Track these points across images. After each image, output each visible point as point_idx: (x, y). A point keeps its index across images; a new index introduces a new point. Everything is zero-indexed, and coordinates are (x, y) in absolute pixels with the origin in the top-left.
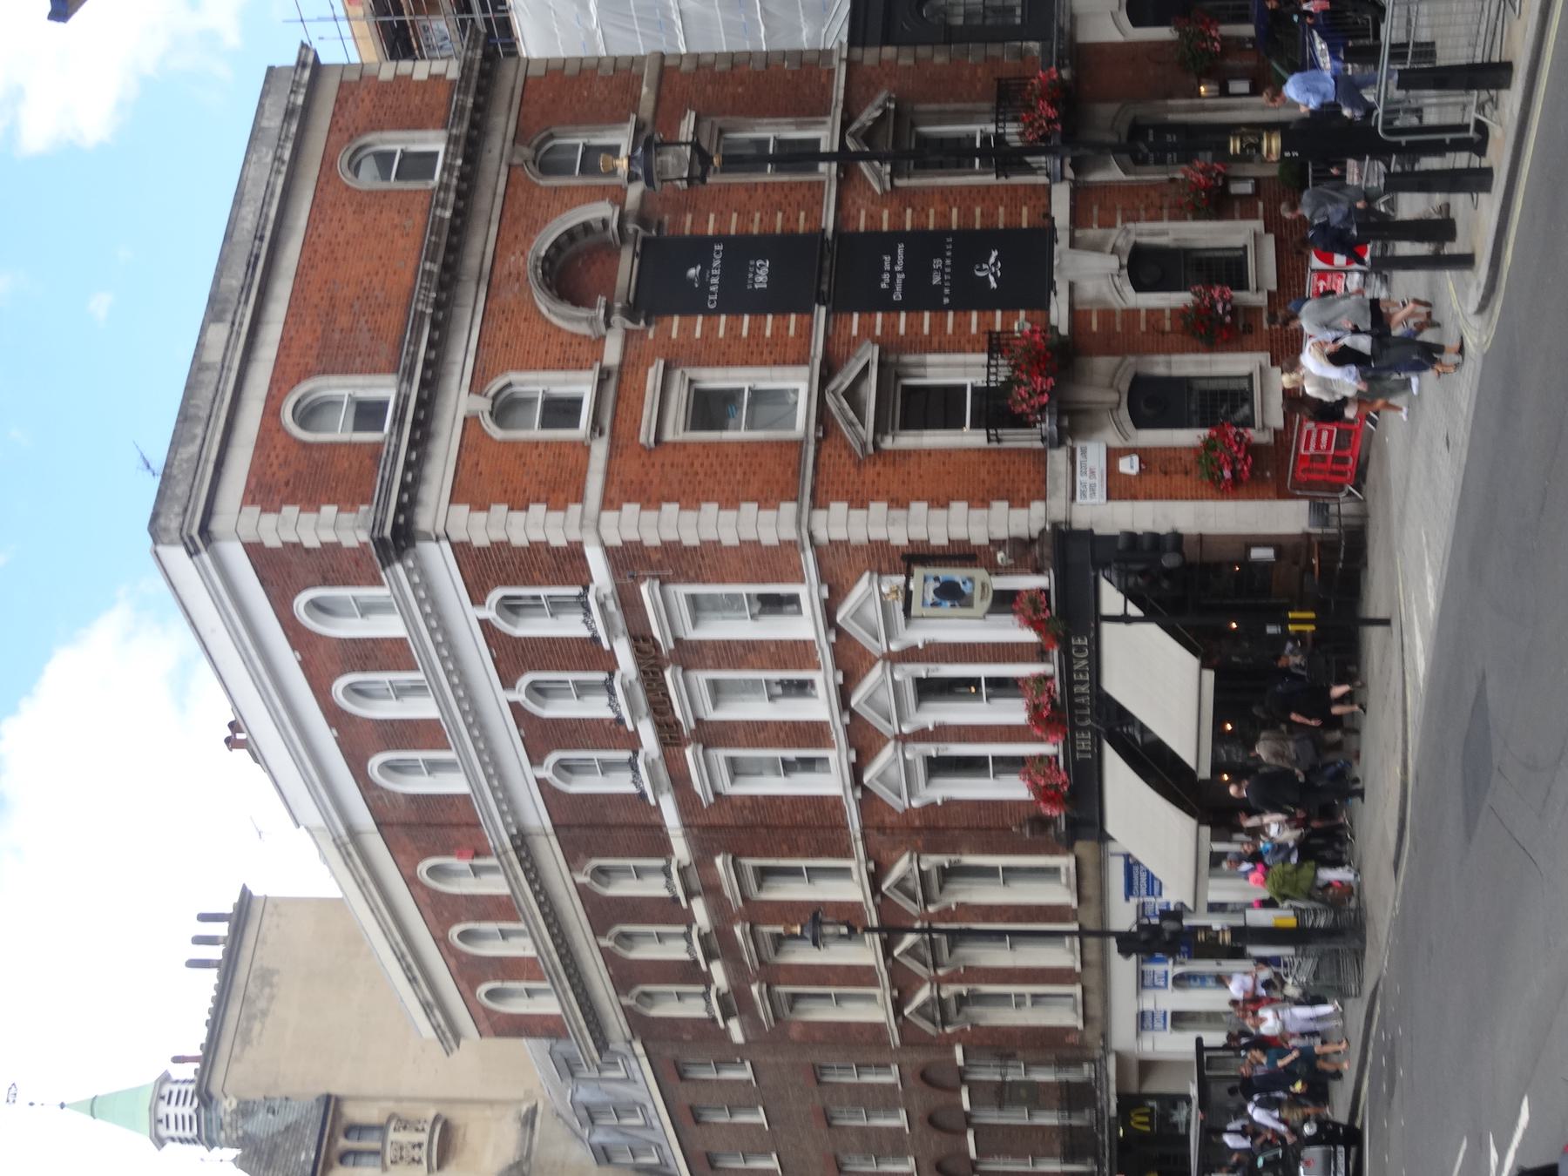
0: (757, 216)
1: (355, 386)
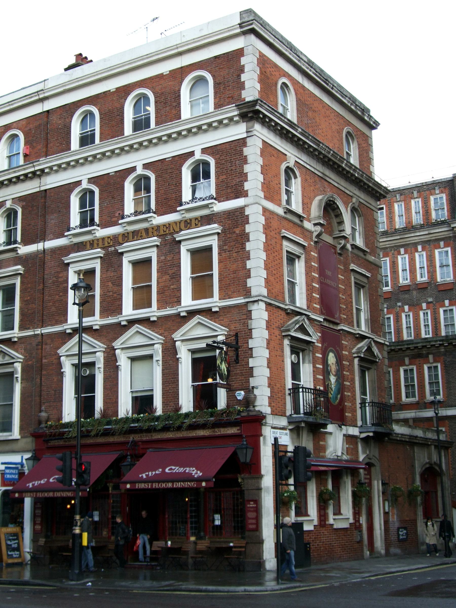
0: (344, 297)
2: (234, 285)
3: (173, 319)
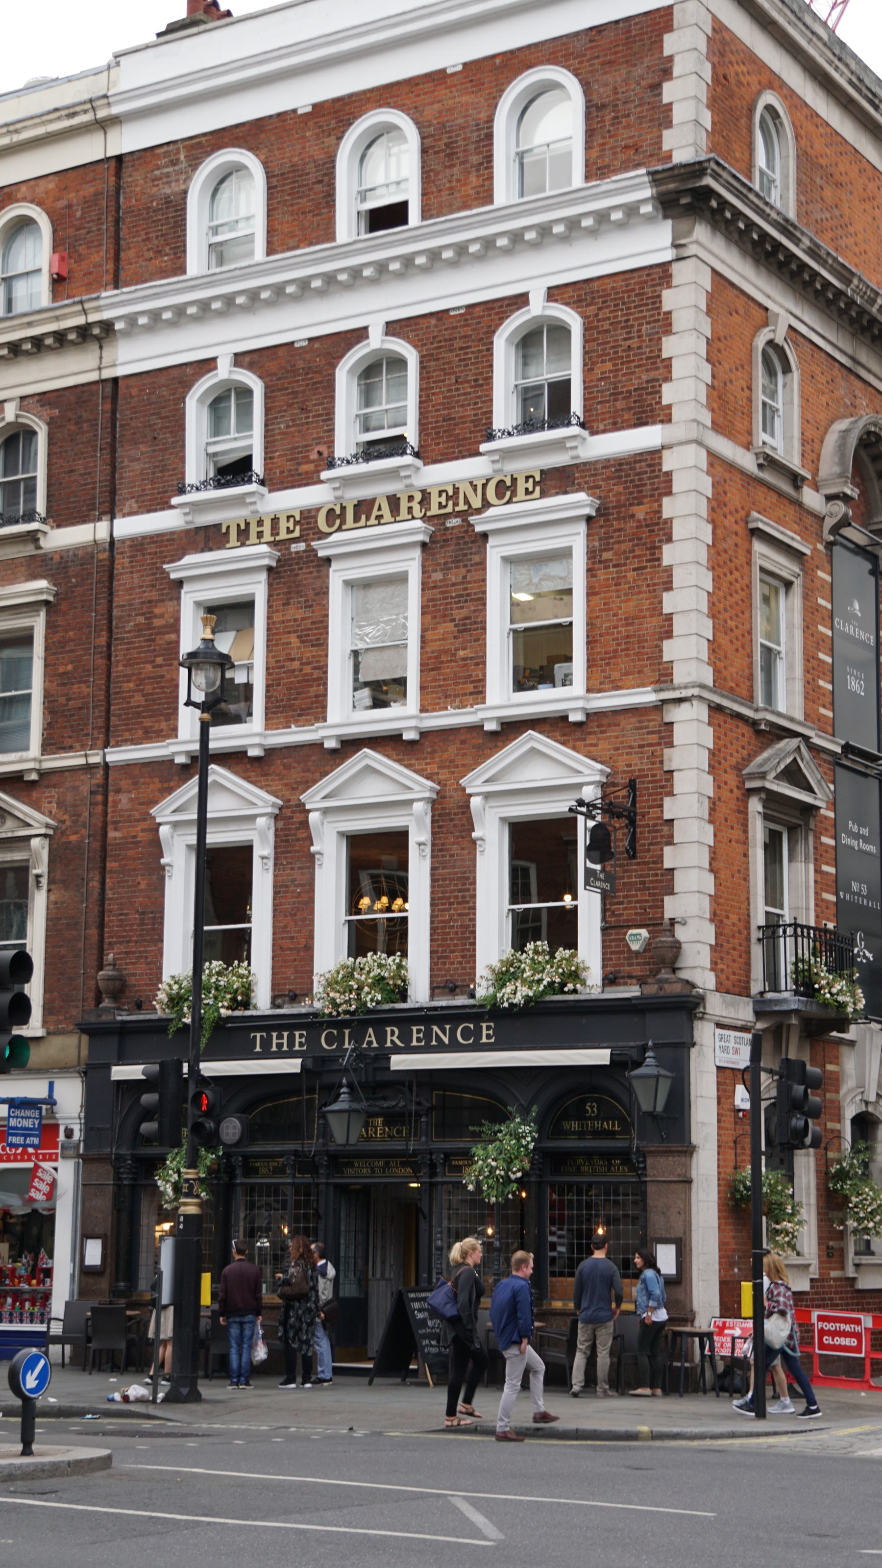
1: (786, 187)
2: (627, 655)
3: (463, 737)
